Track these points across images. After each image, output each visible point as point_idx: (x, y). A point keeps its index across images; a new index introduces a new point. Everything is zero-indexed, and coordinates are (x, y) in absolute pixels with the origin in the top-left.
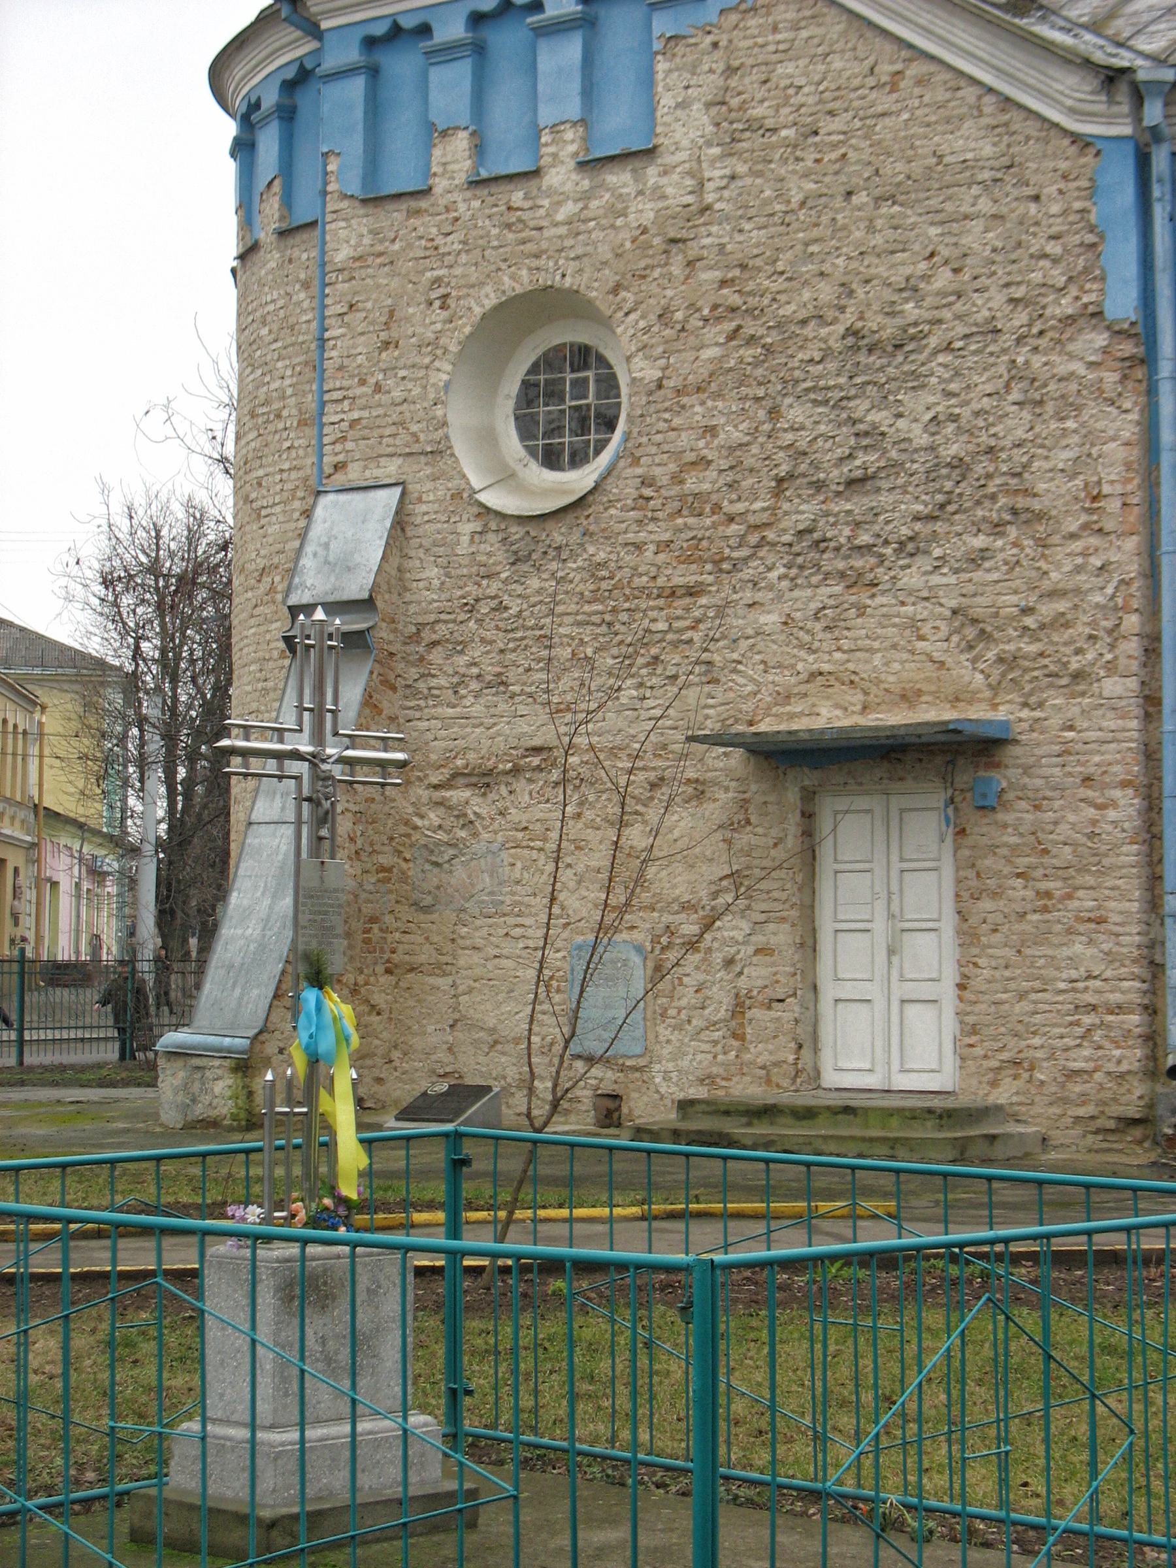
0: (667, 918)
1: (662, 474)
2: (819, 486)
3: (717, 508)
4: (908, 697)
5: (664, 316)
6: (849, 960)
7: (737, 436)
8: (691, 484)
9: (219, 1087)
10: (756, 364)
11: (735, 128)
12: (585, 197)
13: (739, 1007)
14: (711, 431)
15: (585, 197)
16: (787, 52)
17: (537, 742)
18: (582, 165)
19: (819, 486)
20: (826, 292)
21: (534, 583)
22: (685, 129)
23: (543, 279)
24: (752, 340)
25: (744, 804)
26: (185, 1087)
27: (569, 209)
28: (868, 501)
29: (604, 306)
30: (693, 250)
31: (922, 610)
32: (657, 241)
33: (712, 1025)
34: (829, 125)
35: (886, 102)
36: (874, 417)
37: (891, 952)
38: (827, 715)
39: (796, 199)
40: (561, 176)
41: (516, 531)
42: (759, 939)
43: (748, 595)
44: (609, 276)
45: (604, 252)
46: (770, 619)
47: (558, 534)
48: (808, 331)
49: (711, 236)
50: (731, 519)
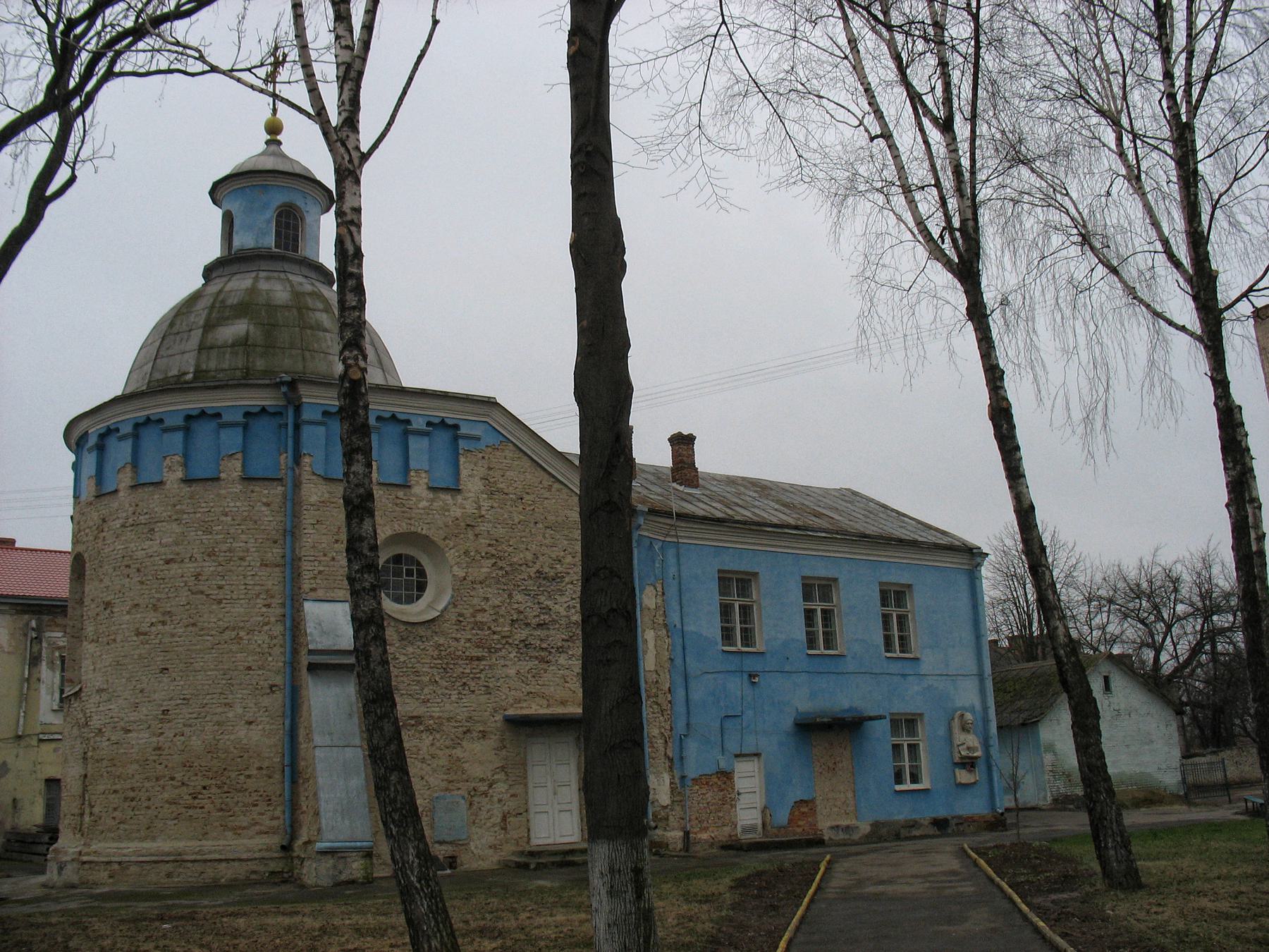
0: (473, 785)
1: (467, 613)
2: (527, 625)
3: (489, 628)
4: (563, 703)
5: (466, 553)
6: (539, 797)
7: (497, 603)
8: (479, 618)
9: (355, 865)
10: (503, 576)
11: (492, 490)
12: (432, 500)
13: (504, 818)
14: (487, 599)
15: (432, 500)
16: (510, 468)
17: (415, 714)
18: (431, 489)
19: (527, 625)
20: (529, 556)
21: (410, 649)
22: (472, 485)
23: (413, 529)
24: (501, 568)
25: (502, 740)
26: (335, 867)
27: (424, 504)
28: (545, 632)
29: (441, 543)
30: (477, 530)
31: (567, 672)
32: (463, 524)
33: (494, 825)
34: (527, 497)
35: (547, 494)
36: (549, 603)
37: (555, 794)
38: (535, 708)
39: (517, 521)
40: (420, 489)
41: (402, 628)
42: (512, 792)
43: (502, 662)
44: (442, 533)
45: (440, 523)
46: (512, 672)
47: (421, 631)
48: (523, 568)
49: (483, 528)
50: (494, 633)
